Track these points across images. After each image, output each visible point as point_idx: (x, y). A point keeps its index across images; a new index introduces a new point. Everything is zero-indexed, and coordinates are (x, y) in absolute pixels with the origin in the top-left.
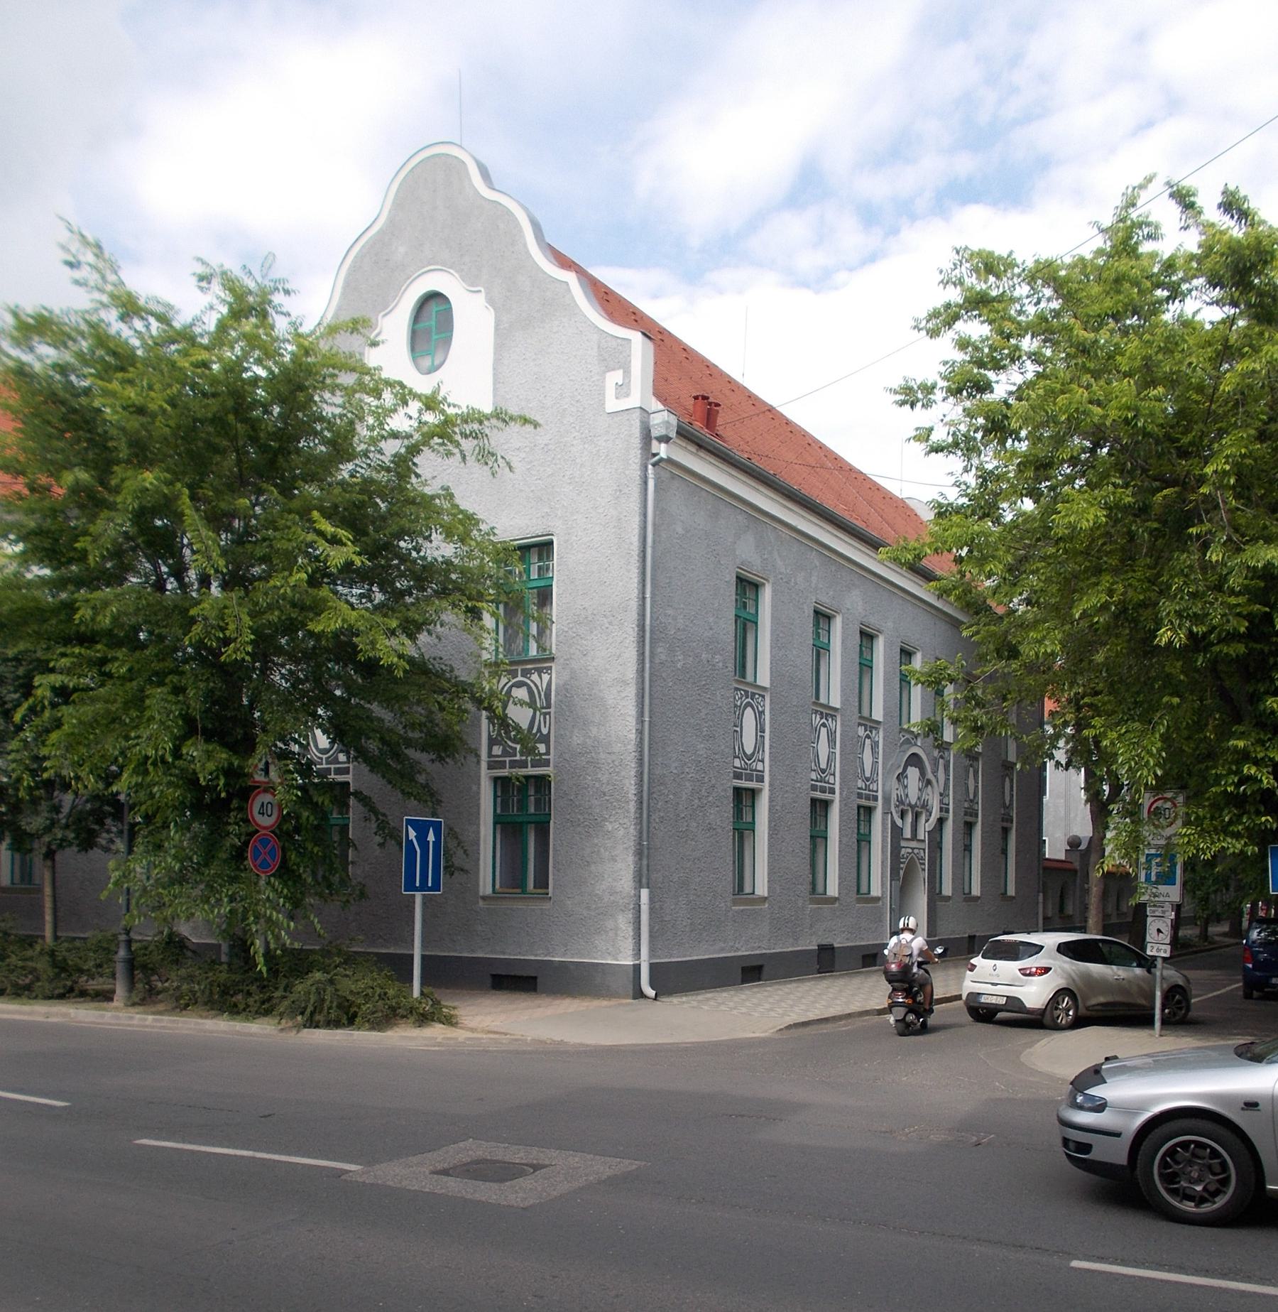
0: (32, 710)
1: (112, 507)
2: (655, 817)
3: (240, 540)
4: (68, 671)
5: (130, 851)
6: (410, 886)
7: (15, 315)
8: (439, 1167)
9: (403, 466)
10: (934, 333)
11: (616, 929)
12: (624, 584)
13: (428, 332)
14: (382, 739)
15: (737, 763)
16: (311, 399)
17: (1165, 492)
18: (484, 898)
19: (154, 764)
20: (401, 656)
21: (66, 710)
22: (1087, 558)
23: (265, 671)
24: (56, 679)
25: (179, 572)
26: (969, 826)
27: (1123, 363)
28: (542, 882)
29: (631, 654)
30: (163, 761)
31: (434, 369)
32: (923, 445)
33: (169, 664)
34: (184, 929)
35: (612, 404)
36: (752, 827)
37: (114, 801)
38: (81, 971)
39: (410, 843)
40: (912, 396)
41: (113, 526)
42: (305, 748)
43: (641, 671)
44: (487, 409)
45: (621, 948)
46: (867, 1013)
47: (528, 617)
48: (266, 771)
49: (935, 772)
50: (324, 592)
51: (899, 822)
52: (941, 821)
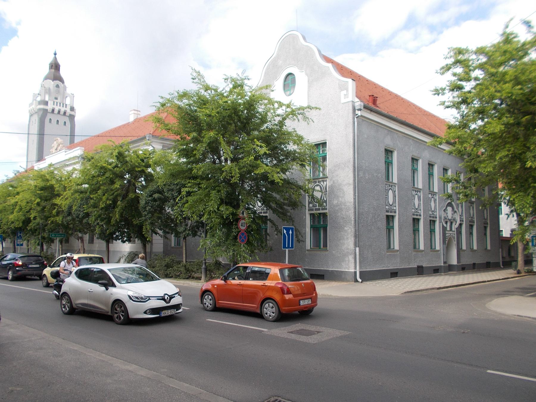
0: (181, 198)
1: (202, 142)
2: (360, 225)
3: (236, 149)
4: (190, 187)
5: (206, 237)
6: (285, 247)
7: (178, 93)
8: (290, 331)
9: (281, 124)
10: (442, 74)
11: (349, 261)
12: (348, 154)
13: (288, 84)
14: (276, 203)
15: (387, 207)
16: (255, 108)
17: (526, 117)
18: (308, 250)
19: (213, 212)
20: (281, 179)
21: (189, 198)
22: (497, 142)
23: (242, 184)
24: (187, 189)
25: (219, 158)
26: (471, 226)
27: (508, 78)
28: (325, 245)
29: (351, 175)
30: (215, 211)
31: (290, 94)
32: (443, 106)
33: (217, 184)
34: (221, 260)
35: (343, 100)
36: (393, 227)
37: (202, 223)
38: (193, 271)
39: (284, 234)
40: (437, 92)
41: (202, 147)
42: (254, 206)
43: (354, 180)
44: (305, 105)
45: (350, 266)
46: (433, 289)
47: (319, 166)
48: (243, 213)
49: (458, 208)
50: (259, 162)
51: (445, 225)
52: (461, 225)
